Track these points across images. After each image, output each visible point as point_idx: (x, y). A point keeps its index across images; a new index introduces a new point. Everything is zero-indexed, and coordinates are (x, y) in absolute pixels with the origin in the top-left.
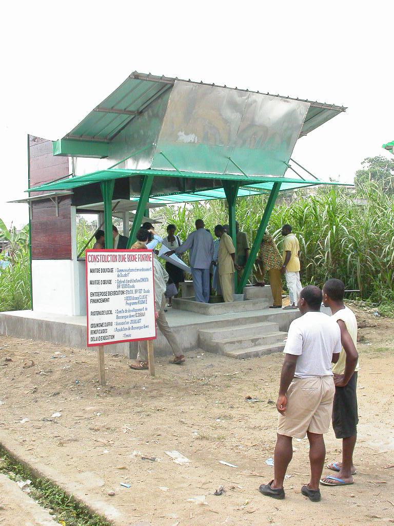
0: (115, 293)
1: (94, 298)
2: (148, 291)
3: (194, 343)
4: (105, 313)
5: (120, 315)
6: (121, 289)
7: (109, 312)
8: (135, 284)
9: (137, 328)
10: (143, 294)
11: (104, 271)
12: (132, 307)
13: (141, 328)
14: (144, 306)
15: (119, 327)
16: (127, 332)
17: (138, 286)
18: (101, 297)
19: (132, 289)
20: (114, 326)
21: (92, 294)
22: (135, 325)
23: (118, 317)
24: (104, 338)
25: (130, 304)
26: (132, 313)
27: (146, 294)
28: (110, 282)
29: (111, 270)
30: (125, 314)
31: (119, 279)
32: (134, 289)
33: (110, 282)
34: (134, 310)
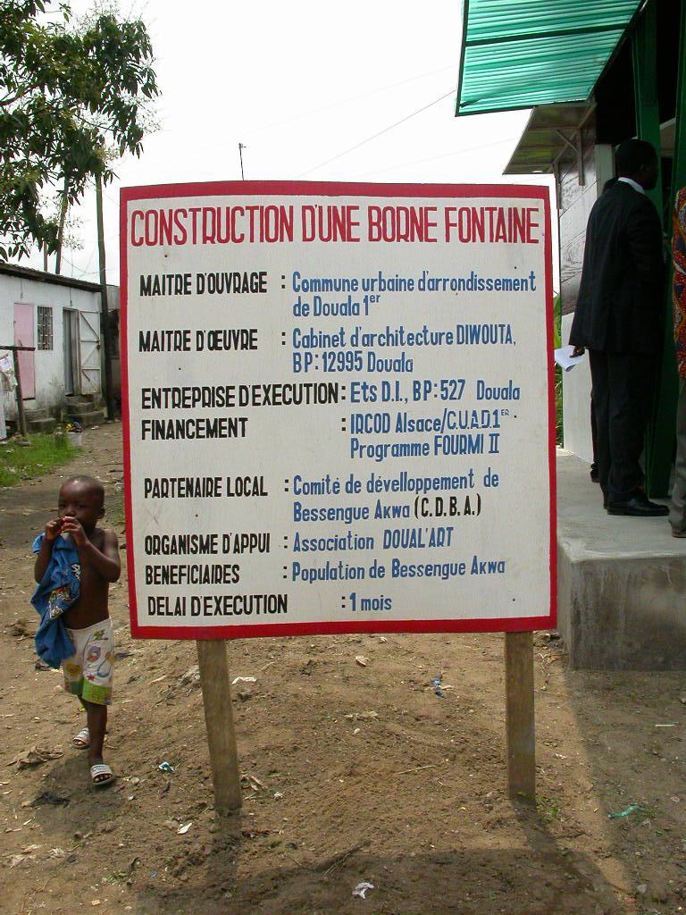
0: (274, 395)
1: (165, 414)
2: (511, 393)
3: (48, 387)
4: (223, 491)
5: (309, 502)
6: (317, 375)
7: (250, 487)
8: (412, 352)
9: (429, 570)
10: (469, 402)
11: (216, 283)
12: (391, 468)
13: (447, 571)
14: (477, 463)
15: (309, 560)
16: (368, 588)
17: (431, 363)
18: (199, 412)
19: (392, 377)
20: (281, 555)
21: (154, 398)
22: (408, 556)
23: (299, 513)
24: (223, 605)
25: (379, 452)
26: (390, 499)
27: (491, 405)
28: (246, 339)
29: (254, 283)
30: (344, 500)
31: (307, 324)
32: (406, 380)
33: (246, 339)
34: (403, 483)
